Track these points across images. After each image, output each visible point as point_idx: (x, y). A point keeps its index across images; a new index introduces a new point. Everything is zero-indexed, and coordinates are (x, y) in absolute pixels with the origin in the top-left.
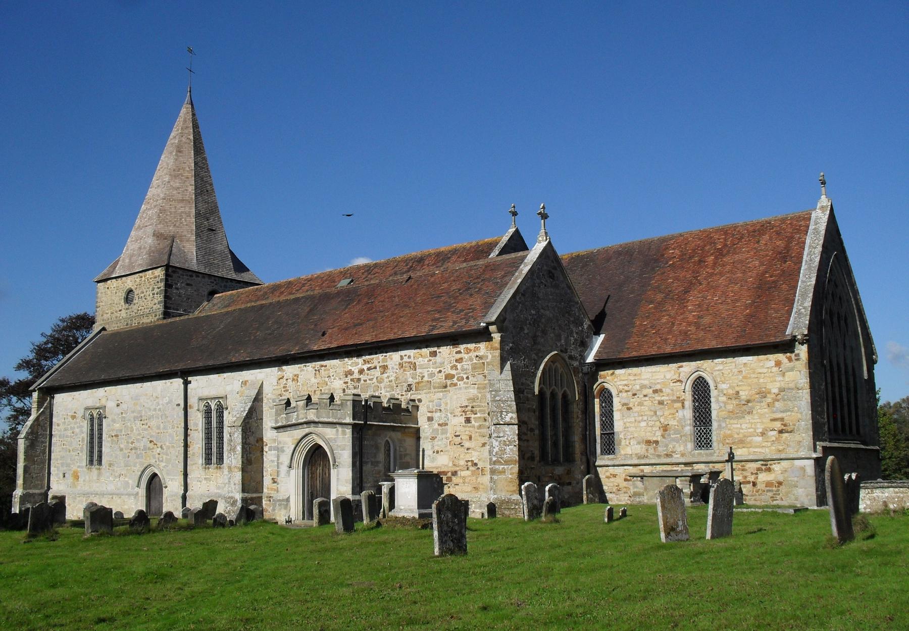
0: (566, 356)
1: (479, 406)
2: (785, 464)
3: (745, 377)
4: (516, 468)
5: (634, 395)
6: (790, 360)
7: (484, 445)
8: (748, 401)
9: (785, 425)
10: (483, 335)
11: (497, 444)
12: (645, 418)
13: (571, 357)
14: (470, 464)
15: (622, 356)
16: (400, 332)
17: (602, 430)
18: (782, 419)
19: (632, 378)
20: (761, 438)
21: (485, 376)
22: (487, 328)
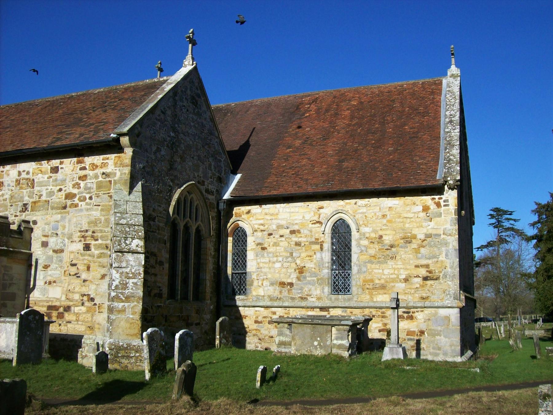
0: (203, 188)
1: (101, 231)
2: (427, 311)
3: (390, 221)
4: (139, 307)
5: (270, 234)
6: (438, 205)
7: (103, 277)
8: (392, 246)
9: (430, 272)
10: (114, 147)
11: (118, 276)
12: (280, 259)
13: (207, 191)
14: (85, 298)
15: (261, 194)
16: (20, 145)
17: (233, 269)
18: (427, 266)
19: (268, 217)
20: (403, 285)
21: (111, 197)
22: (117, 140)
